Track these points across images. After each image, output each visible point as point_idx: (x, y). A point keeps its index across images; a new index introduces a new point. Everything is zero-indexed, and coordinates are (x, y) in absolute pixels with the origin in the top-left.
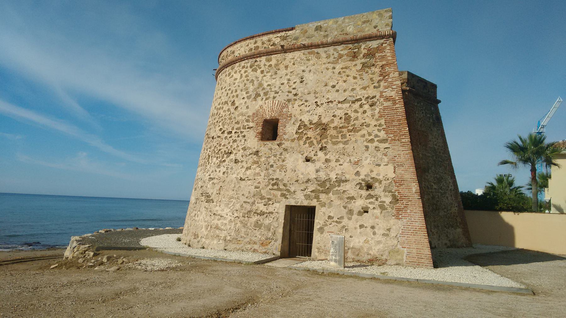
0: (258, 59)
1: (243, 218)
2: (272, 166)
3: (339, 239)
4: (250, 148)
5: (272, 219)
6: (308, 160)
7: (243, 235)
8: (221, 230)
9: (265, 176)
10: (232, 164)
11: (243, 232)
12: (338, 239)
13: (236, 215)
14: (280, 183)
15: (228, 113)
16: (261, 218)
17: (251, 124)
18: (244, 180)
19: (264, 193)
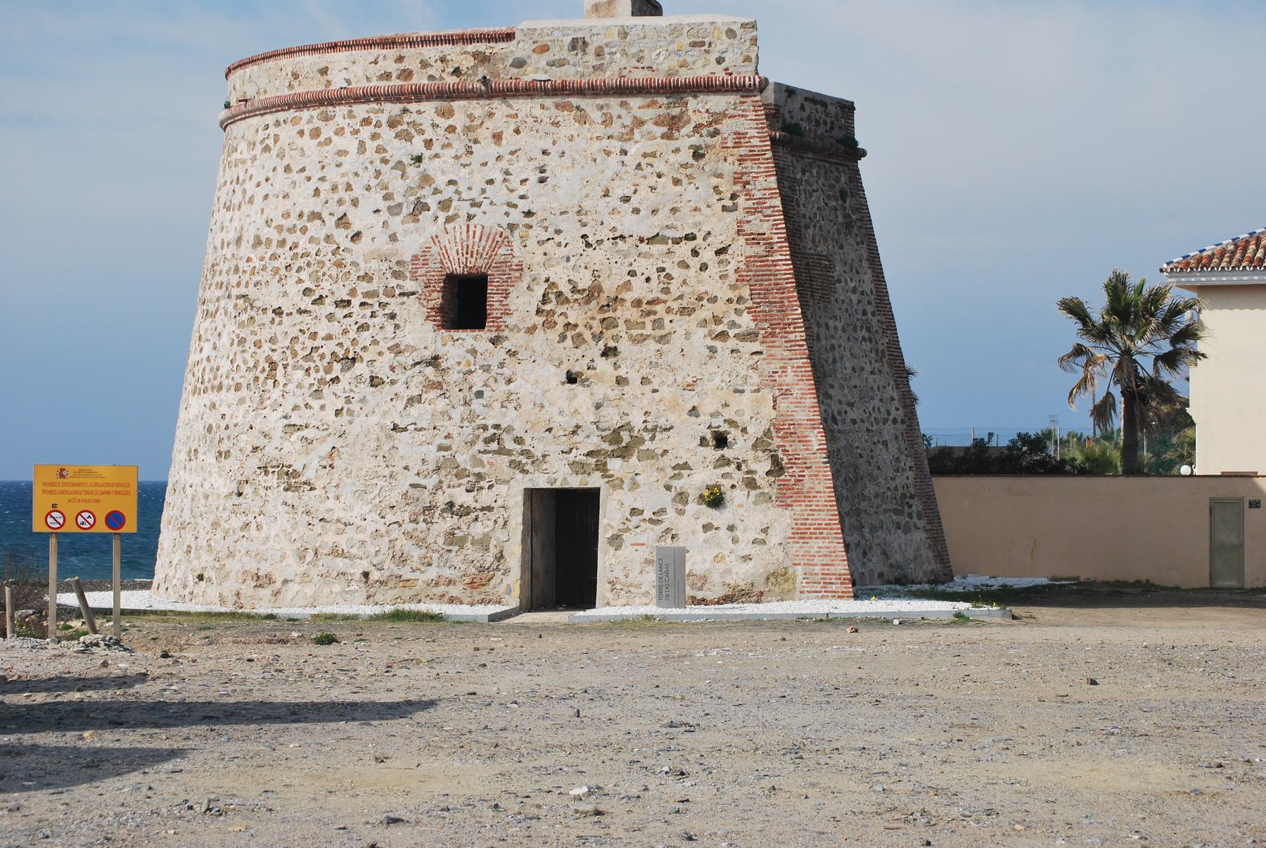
1: (413, 525)
2: (480, 394)
4: (414, 349)
6: (572, 379)
8: (352, 558)
10: (365, 389)
11: (416, 558)
13: (391, 517)
14: (504, 436)
17: (409, 285)
18: (405, 429)
19: (463, 459)
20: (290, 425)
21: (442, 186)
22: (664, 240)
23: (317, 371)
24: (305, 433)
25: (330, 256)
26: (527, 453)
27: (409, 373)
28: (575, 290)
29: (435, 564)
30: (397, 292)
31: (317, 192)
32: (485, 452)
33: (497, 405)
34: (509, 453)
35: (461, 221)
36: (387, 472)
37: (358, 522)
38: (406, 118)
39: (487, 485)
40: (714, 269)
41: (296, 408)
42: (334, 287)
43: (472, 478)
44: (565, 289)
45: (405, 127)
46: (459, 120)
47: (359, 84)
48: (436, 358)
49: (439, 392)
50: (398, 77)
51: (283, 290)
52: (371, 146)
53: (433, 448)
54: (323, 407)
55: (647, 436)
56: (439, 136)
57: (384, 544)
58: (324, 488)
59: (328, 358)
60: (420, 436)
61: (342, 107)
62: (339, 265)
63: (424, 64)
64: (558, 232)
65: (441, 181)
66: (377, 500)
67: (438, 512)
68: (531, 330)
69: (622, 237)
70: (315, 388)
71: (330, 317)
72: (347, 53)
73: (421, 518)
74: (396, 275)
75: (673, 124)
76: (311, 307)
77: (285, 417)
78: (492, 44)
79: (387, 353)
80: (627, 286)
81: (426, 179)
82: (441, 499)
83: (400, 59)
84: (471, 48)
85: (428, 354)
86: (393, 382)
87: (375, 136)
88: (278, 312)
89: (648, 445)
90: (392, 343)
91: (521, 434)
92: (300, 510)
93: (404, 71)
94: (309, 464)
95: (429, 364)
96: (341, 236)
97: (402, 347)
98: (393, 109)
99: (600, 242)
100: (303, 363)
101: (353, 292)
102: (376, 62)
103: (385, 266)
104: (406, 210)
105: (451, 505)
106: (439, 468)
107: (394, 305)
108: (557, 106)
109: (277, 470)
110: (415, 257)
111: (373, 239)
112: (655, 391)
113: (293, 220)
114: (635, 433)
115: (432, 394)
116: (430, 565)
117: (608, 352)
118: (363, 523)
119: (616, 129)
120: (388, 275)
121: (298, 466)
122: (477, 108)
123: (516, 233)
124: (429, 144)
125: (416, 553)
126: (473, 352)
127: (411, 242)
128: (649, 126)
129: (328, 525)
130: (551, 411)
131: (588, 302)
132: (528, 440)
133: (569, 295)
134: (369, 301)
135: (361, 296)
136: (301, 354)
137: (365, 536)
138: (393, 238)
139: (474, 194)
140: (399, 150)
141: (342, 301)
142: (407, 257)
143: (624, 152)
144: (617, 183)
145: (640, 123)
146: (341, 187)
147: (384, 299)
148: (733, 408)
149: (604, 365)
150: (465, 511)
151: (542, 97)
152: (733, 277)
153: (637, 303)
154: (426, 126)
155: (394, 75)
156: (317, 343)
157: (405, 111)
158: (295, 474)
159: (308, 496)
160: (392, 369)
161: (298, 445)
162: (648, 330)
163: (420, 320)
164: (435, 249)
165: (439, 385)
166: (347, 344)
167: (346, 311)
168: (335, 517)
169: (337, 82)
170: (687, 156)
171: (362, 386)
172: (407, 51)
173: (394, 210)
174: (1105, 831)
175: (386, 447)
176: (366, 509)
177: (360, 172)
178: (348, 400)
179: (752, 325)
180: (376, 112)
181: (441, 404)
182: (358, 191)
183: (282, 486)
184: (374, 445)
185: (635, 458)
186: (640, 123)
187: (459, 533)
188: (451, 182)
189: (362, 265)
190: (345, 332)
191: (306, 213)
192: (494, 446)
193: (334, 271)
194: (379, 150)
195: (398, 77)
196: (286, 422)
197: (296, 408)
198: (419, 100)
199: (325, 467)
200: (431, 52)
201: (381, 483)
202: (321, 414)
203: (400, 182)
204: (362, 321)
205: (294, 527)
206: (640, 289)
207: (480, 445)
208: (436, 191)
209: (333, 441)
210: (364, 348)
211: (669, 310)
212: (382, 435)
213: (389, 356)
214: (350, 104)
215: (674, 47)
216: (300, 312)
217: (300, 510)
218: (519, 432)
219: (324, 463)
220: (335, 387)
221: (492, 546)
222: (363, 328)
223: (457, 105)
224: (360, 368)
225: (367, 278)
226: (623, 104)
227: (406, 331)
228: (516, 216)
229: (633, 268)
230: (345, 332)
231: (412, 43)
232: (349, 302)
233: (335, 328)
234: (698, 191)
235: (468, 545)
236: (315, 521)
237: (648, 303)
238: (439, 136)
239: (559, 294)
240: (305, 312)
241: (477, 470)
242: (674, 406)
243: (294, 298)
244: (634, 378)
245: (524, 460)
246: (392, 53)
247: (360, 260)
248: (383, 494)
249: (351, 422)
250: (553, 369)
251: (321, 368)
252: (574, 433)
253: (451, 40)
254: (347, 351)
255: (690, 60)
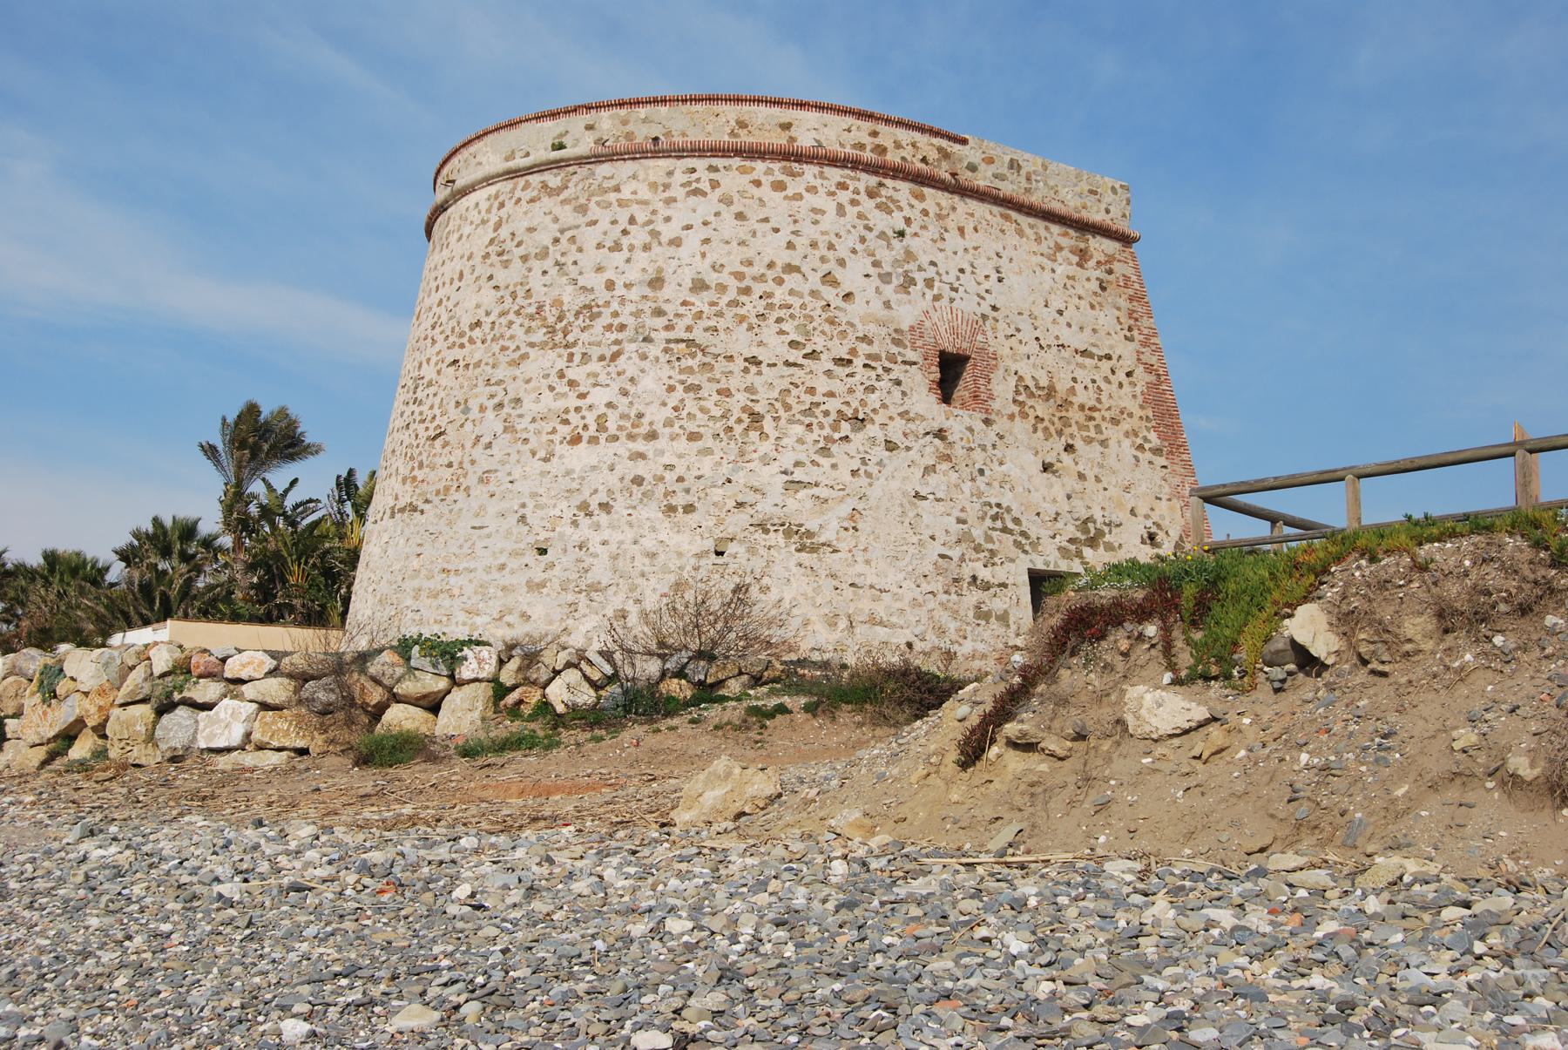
0: (888, 182)
1: (946, 596)
2: (981, 472)
3: (852, 676)
4: (923, 418)
5: (1007, 600)
6: (1046, 468)
7: (954, 637)
8: (893, 626)
9: (972, 495)
10: (880, 452)
11: (952, 630)
12: (846, 674)
13: (926, 587)
14: (1005, 515)
15: (668, 232)
16: (985, 596)
17: (911, 355)
18: (925, 498)
19: (978, 533)
20: (793, 482)
21: (925, 265)
22: (1091, 356)
23: (821, 427)
24: (815, 491)
25: (819, 311)
26: (1023, 534)
27: (922, 442)
28: (1039, 388)
29: (969, 637)
30: (900, 359)
31: (790, 246)
32: (994, 529)
33: (996, 484)
34: (1011, 532)
35: (945, 302)
36: (915, 539)
37: (894, 589)
38: (883, 192)
39: (999, 562)
40: (1127, 388)
41: (797, 464)
42: (830, 344)
43: (986, 554)
44: (1031, 384)
45: (884, 200)
46: (929, 205)
47: (833, 147)
48: (941, 430)
49: (951, 465)
50: (872, 151)
51: (758, 339)
52: (851, 211)
53: (953, 520)
54: (834, 466)
55: (1106, 529)
56: (915, 214)
57: (922, 613)
58: (850, 551)
59: (834, 416)
60: (940, 507)
61: (812, 167)
62: (831, 322)
63: (898, 145)
64: (1018, 330)
65: (924, 260)
66: (910, 568)
67: (966, 585)
68: (1012, 417)
69: (1063, 346)
70: (821, 444)
71: (828, 373)
72: (817, 114)
73: (953, 590)
74: (897, 342)
75: (1083, 255)
76: (800, 361)
77: (785, 473)
78: (951, 144)
79: (898, 419)
80: (1072, 391)
81: (909, 255)
82: (966, 572)
83: (874, 134)
84: (937, 141)
85: (936, 426)
86: (908, 449)
87: (854, 202)
88: (754, 361)
89: (1107, 538)
90: (901, 409)
91: (1018, 515)
92: (823, 573)
93: (878, 146)
94: (828, 526)
95: (936, 436)
96: (829, 293)
97: (912, 415)
98: (873, 180)
99: (1049, 346)
100: (802, 418)
101: (853, 351)
102: (849, 131)
103: (884, 331)
104: (896, 281)
105: (974, 578)
106: (959, 541)
107: (898, 371)
108: (1002, 215)
109: (781, 528)
110: (912, 328)
111: (868, 302)
112: (1105, 489)
113: (759, 269)
114: (1098, 526)
115: (945, 466)
116: (965, 638)
117: (1069, 448)
118: (900, 591)
119: (1044, 248)
120: (889, 341)
121: (812, 525)
122: (945, 199)
123: (987, 323)
124: (908, 221)
125: (952, 626)
126: (971, 430)
127: (907, 313)
128: (1066, 253)
129: (861, 591)
130: (1036, 497)
131: (1047, 400)
132: (1024, 522)
133: (1034, 390)
134: (873, 364)
135: (863, 357)
136: (796, 408)
137: (904, 604)
138: (887, 305)
139: (951, 278)
140: (880, 221)
141: (841, 359)
142: (905, 327)
143: (1053, 271)
144: (1053, 296)
145: (1059, 248)
146: (822, 246)
147: (888, 365)
148: (1157, 512)
149: (1067, 459)
150: (987, 587)
151: (990, 203)
152: (1140, 399)
153: (1082, 407)
154: (903, 204)
155: (868, 148)
156: (816, 399)
157: (881, 185)
158: (810, 534)
159: (830, 559)
160: (905, 435)
161: (809, 504)
162: (1092, 433)
163: (925, 391)
164: (928, 324)
165: (948, 458)
166: (855, 404)
167: (848, 370)
168: (869, 583)
169: (805, 141)
170: (1094, 286)
171: (877, 448)
172: (881, 127)
173: (886, 278)
174: (624, 793)
175: (911, 514)
176: (901, 576)
177: (843, 233)
178: (864, 462)
179: (1158, 442)
180: (852, 179)
181: (954, 476)
182: (843, 251)
183: (794, 547)
184: (899, 511)
185: (1102, 548)
186: (1059, 248)
187: (985, 608)
188: (933, 264)
189: (860, 326)
190: (851, 391)
191: (779, 263)
192: (999, 524)
193: (827, 328)
194: (860, 216)
195: (872, 151)
196: (786, 478)
197: (797, 464)
198: (894, 178)
199: (846, 529)
200: (904, 135)
201: (912, 550)
202: (837, 470)
203: (887, 252)
204: (868, 383)
205: (818, 590)
206: (1082, 397)
207: (988, 522)
208: (920, 269)
209: (852, 503)
210: (874, 410)
211: (1104, 419)
212: (905, 501)
213: (899, 423)
214: (821, 165)
215: (1078, 189)
216: (788, 364)
217: (823, 573)
218: (1015, 513)
219: (846, 524)
220: (845, 446)
221: (1011, 622)
222: (871, 389)
223: (927, 191)
224: (872, 430)
225: (865, 339)
226: (1047, 228)
227: (914, 400)
228: (986, 309)
229: (1075, 375)
230: (851, 391)
231: (888, 121)
232: (850, 362)
233: (836, 386)
234: (1106, 319)
235: (993, 620)
236: (845, 586)
237: (1090, 409)
238: (915, 214)
239: (1027, 387)
240: (795, 365)
241: (990, 546)
242: (1120, 505)
243: (775, 347)
244: (1090, 475)
245: (1025, 543)
246: (867, 126)
247: (856, 321)
248: (915, 562)
249: (870, 485)
250: (1033, 457)
251: (826, 425)
252: (1055, 519)
253: (921, 129)
254: (856, 411)
255: (1089, 204)
